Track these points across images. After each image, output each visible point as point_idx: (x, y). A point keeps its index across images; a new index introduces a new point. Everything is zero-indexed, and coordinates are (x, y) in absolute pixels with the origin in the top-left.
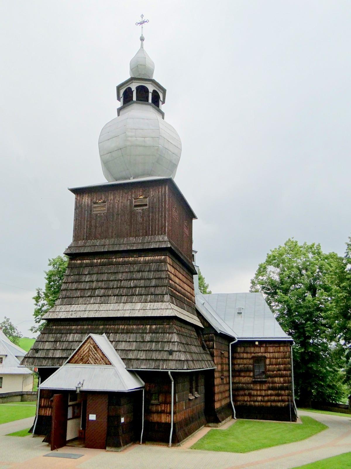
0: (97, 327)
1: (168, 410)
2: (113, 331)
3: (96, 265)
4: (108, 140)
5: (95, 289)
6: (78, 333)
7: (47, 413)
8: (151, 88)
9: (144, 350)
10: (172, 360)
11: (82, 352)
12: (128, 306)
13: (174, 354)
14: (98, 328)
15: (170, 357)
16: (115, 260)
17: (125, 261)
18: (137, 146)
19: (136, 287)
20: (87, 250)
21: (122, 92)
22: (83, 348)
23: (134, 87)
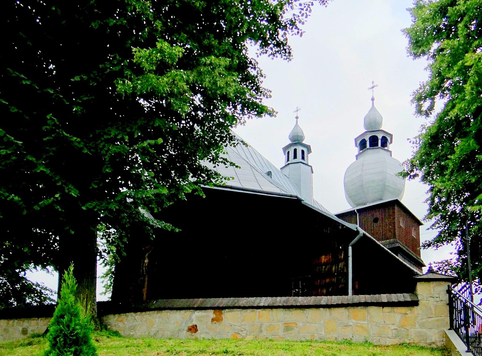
8: (380, 136)
21: (359, 142)
23: (367, 138)
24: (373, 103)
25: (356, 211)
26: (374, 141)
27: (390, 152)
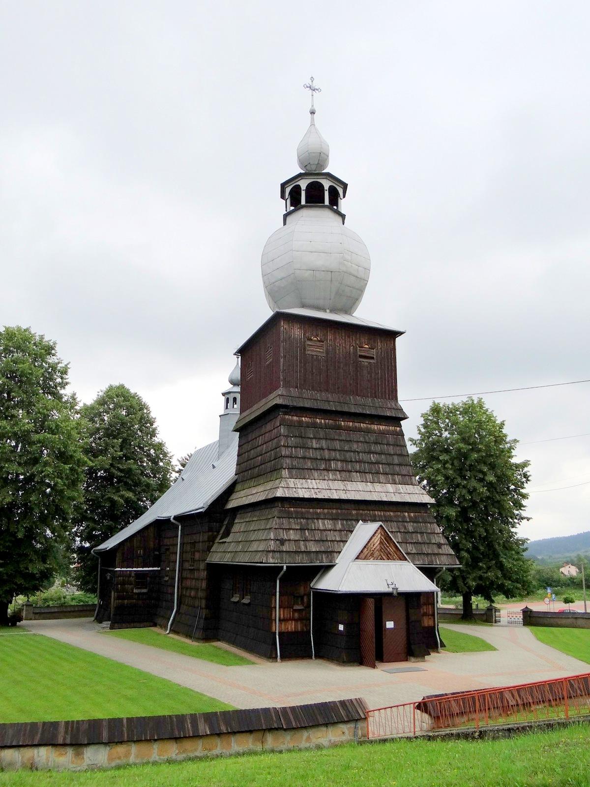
0: (349, 512)
1: (431, 612)
2: (370, 518)
3: (321, 427)
4: (312, 252)
5: (329, 460)
6: (327, 519)
7: (289, 628)
8: (326, 184)
9: (411, 543)
10: (443, 554)
11: (372, 544)
12: (378, 487)
13: (443, 547)
14: (350, 514)
15: (441, 551)
16: (343, 423)
17: (356, 427)
18: (350, 274)
19: (378, 463)
20: (307, 404)
21: (288, 190)
22: (373, 540)
23: (303, 184)
24: (313, 120)
25: (125, 721)
26: (315, 196)
27: (343, 217)
